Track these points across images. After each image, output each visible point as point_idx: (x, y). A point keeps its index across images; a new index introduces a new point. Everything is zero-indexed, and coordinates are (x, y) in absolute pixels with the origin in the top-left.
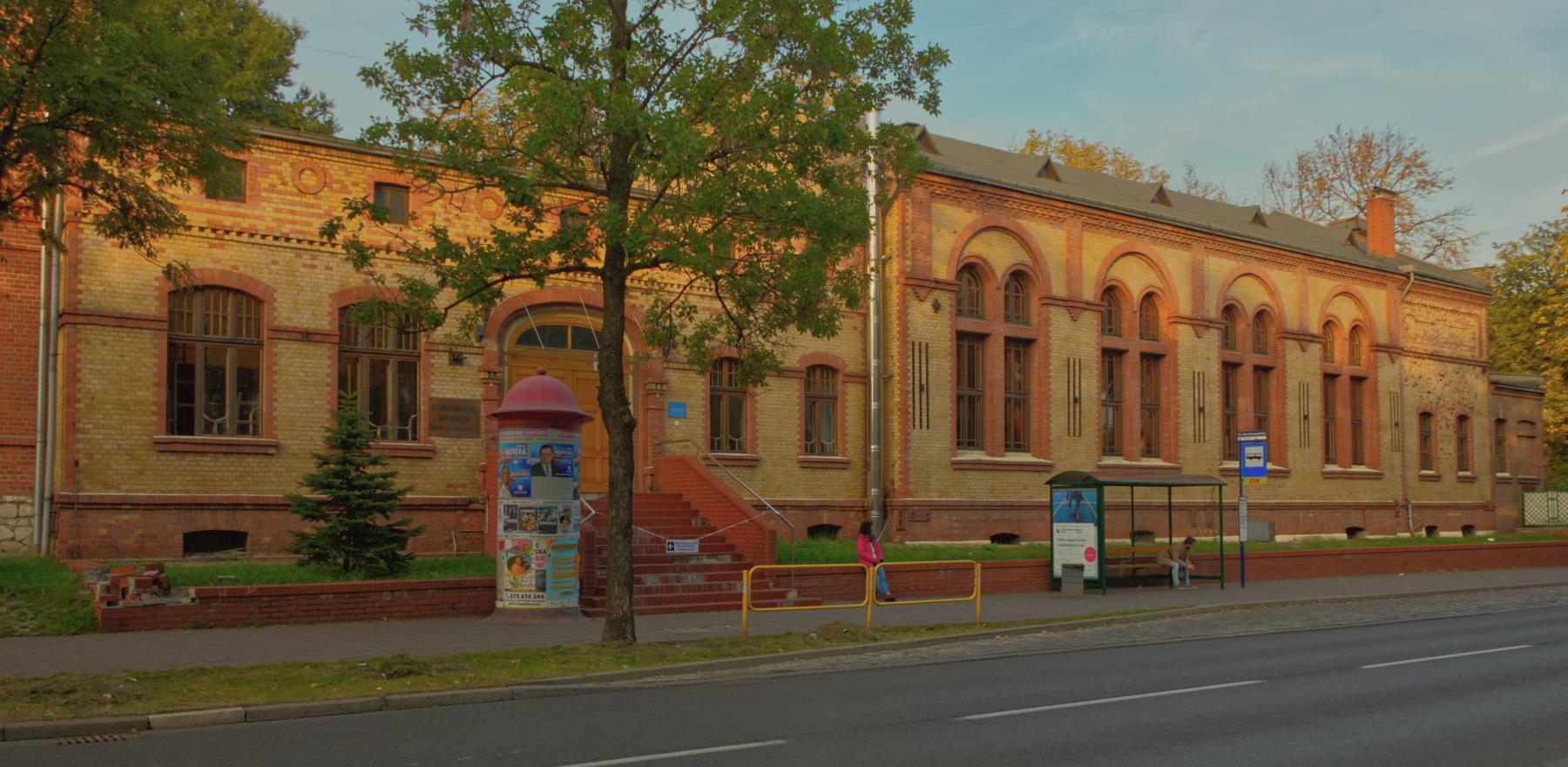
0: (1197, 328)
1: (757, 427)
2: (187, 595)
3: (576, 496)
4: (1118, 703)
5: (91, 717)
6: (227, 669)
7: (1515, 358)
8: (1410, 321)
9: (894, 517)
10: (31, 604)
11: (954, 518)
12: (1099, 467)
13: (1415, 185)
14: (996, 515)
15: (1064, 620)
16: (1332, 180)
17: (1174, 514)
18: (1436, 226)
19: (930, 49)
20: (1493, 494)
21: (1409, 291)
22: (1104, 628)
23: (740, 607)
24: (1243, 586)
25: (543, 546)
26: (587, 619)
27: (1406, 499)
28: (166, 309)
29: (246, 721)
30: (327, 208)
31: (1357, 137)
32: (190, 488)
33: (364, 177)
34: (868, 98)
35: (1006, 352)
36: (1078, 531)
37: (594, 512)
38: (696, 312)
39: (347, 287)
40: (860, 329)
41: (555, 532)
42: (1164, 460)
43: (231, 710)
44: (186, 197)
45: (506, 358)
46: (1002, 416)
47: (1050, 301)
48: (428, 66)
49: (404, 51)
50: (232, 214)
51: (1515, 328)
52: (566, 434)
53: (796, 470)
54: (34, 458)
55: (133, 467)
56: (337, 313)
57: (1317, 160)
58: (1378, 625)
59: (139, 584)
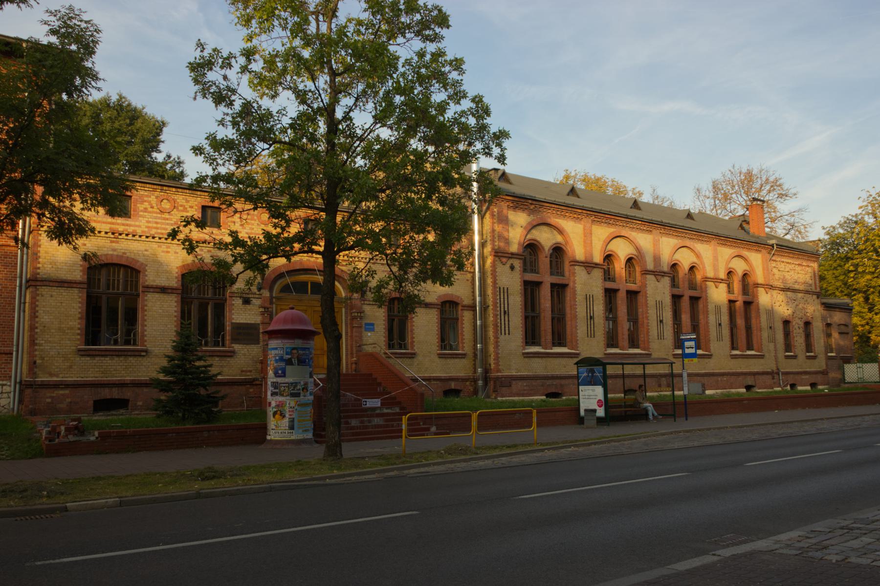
0: (657, 276)
1: (414, 336)
2: (94, 435)
3: (311, 376)
4: (606, 487)
5: (35, 505)
6: (113, 477)
7: (837, 289)
8: (775, 271)
9: (491, 384)
10: (7, 442)
11: (525, 384)
12: (605, 354)
13: (776, 196)
14: (549, 382)
15: (584, 441)
16: (731, 194)
17: (647, 379)
18: (789, 218)
19: (499, 130)
20: (827, 365)
21: (774, 254)
22: (606, 445)
23: (401, 437)
24: (687, 419)
25: (293, 404)
26: (317, 445)
27: (778, 369)
28: (86, 277)
29: (120, 506)
30: (175, 220)
31: (744, 170)
32: (98, 375)
33: (196, 203)
34: (467, 157)
35: (552, 292)
36: (593, 390)
37: (321, 385)
38: (376, 274)
39: (186, 263)
40: (470, 281)
41: (299, 397)
42: (642, 350)
43: (112, 500)
44: (98, 218)
45: (274, 300)
46: (551, 327)
47: (575, 263)
48: (228, 145)
49: (215, 137)
50: (123, 225)
51: (837, 273)
52: (305, 342)
53: (437, 359)
54: (12, 360)
55: (66, 364)
56: (180, 277)
57: (723, 183)
58: (759, 440)
59: (67, 429)
